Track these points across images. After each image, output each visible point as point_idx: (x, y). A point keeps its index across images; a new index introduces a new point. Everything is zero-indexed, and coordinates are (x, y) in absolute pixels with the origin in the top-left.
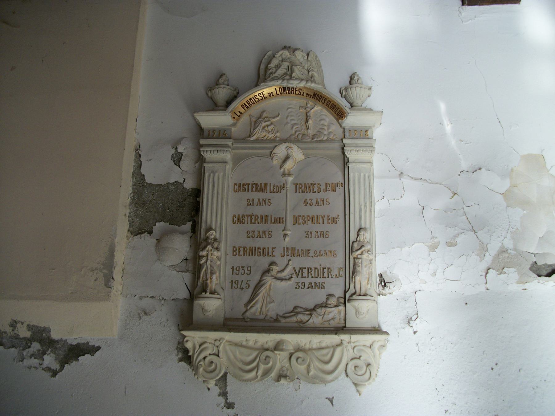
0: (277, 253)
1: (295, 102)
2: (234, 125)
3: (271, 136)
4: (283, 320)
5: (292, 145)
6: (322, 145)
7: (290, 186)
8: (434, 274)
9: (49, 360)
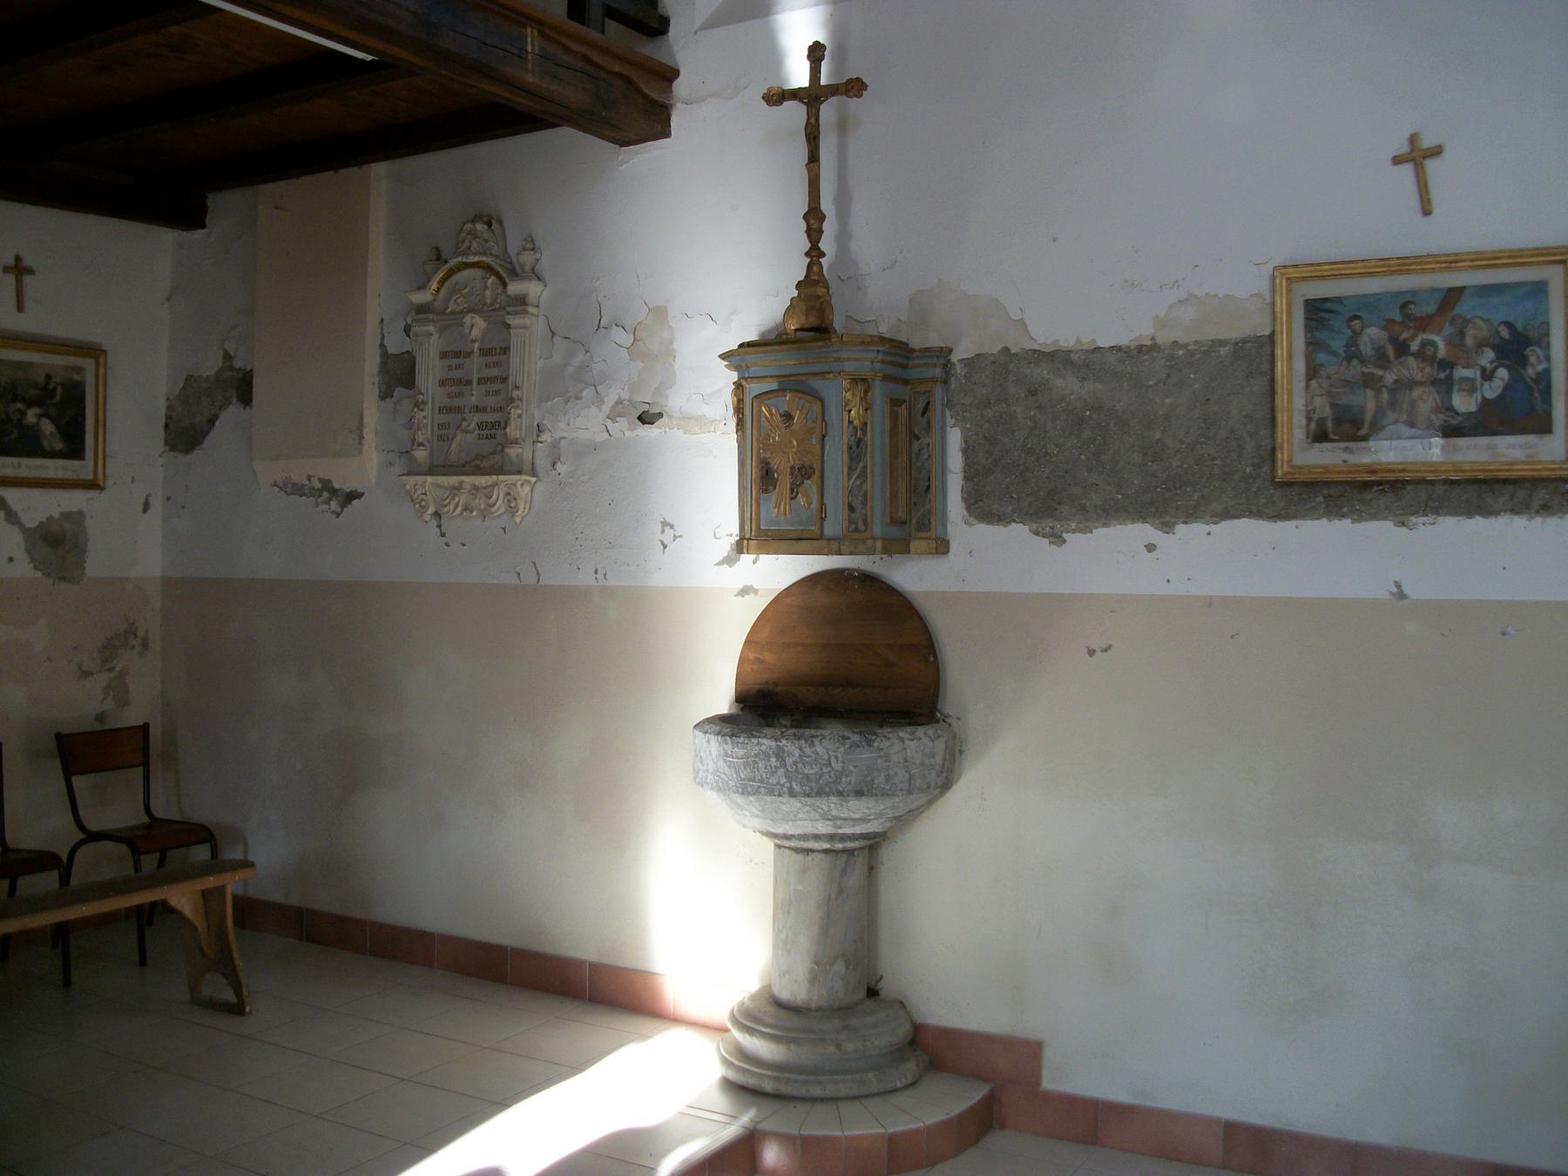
9: (334, 505)
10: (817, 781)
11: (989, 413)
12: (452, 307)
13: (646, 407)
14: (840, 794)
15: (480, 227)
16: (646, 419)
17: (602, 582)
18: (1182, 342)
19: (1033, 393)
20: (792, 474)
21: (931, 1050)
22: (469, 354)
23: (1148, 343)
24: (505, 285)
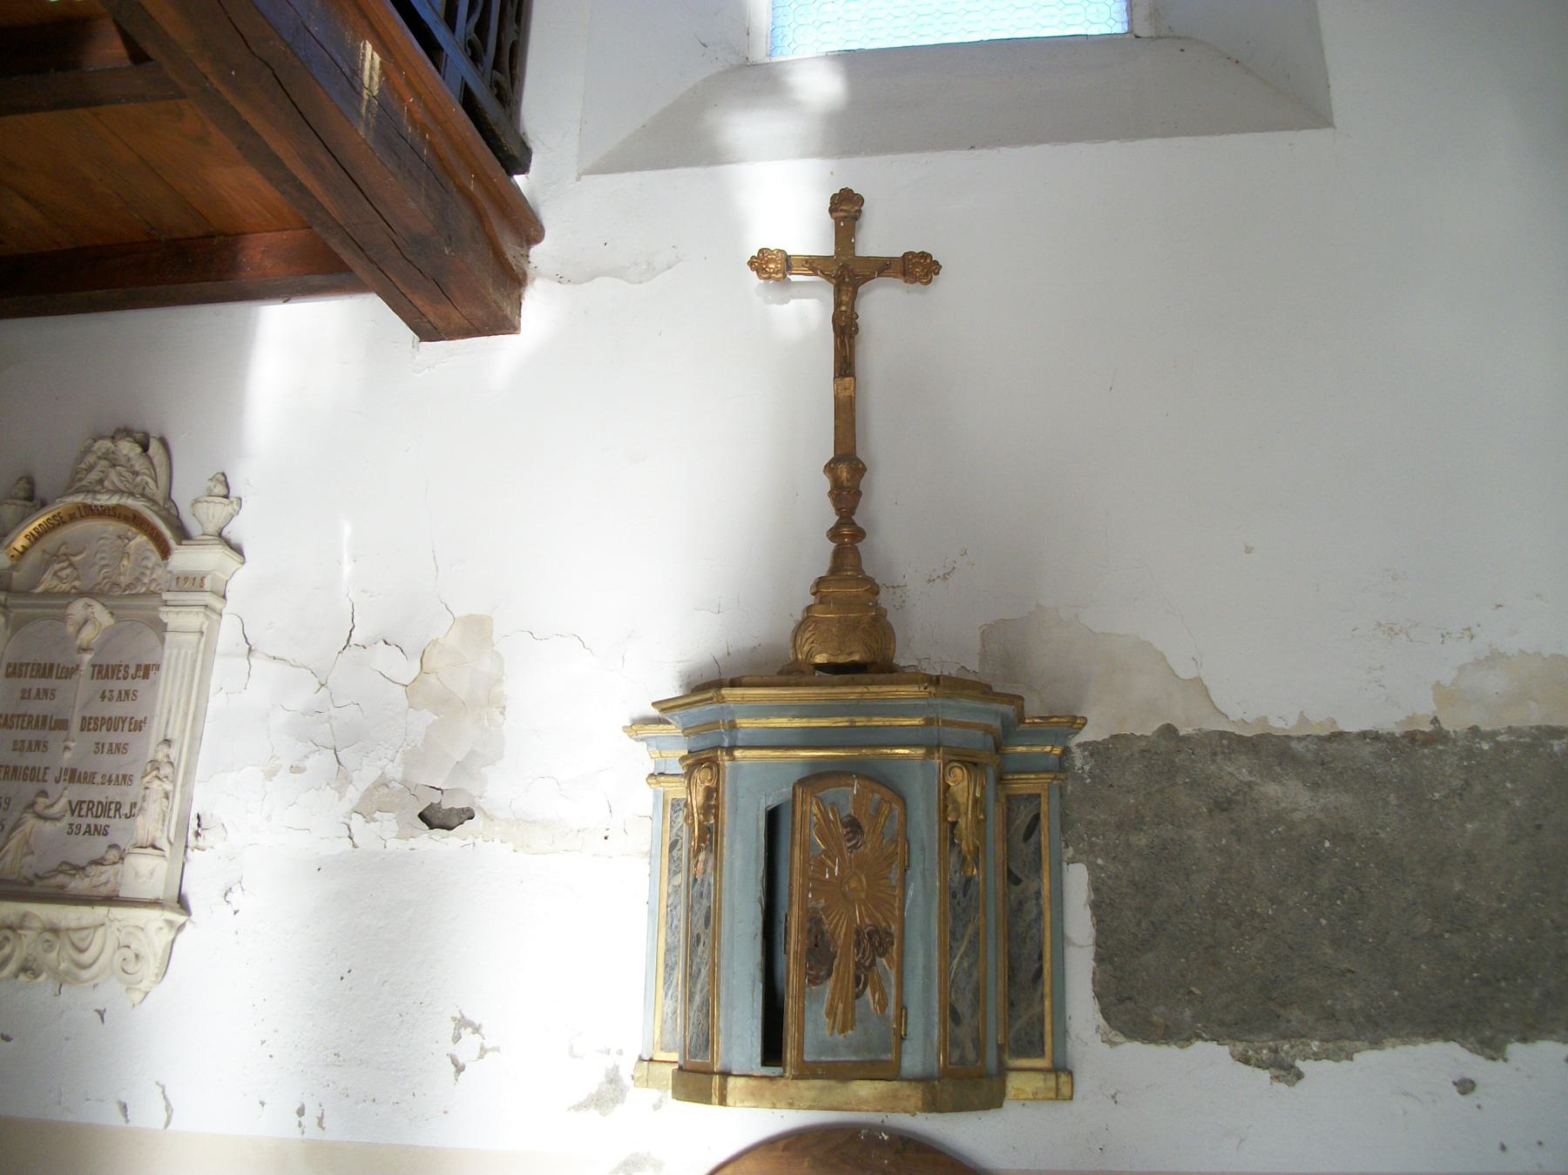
0: (50, 777)
1: (111, 528)
2: (13, 567)
3: (65, 587)
4: (38, 883)
5: (93, 602)
6: (137, 602)
7: (85, 668)
8: (269, 818)
11: (1140, 840)
12: (48, 582)
13: (436, 798)
15: (127, 448)
16: (435, 819)
17: (313, 1132)
18: (1484, 728)
19: (1223, 805)
20: (858, 944)
22: (70, 672)
23: (1428, 728)
24: (165, 552)
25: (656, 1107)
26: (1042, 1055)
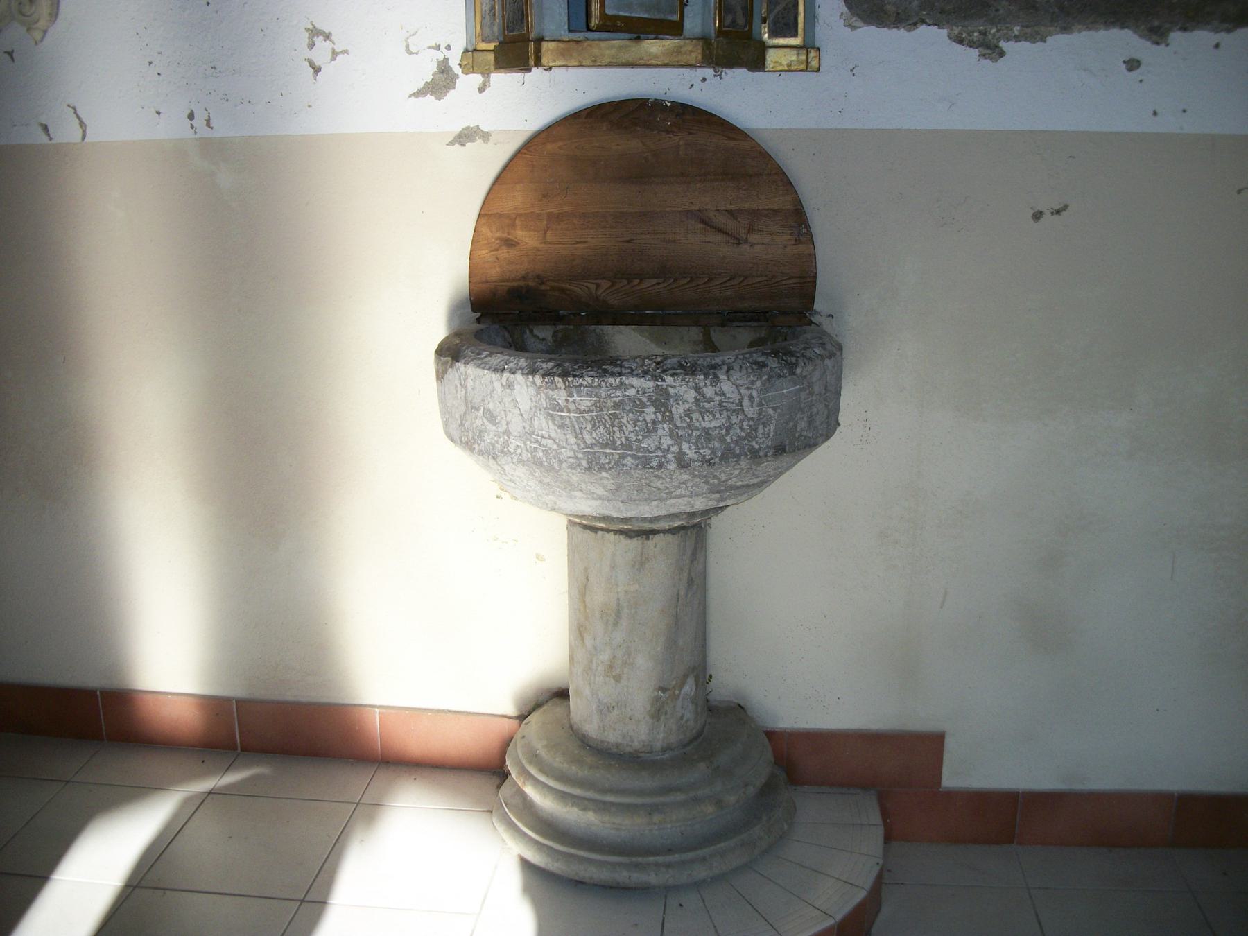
10: (722, 440)
14: (755, 455)
17: (204, 132)
21: (800, 765)
25: (482, 89)
26: (795, 35)
